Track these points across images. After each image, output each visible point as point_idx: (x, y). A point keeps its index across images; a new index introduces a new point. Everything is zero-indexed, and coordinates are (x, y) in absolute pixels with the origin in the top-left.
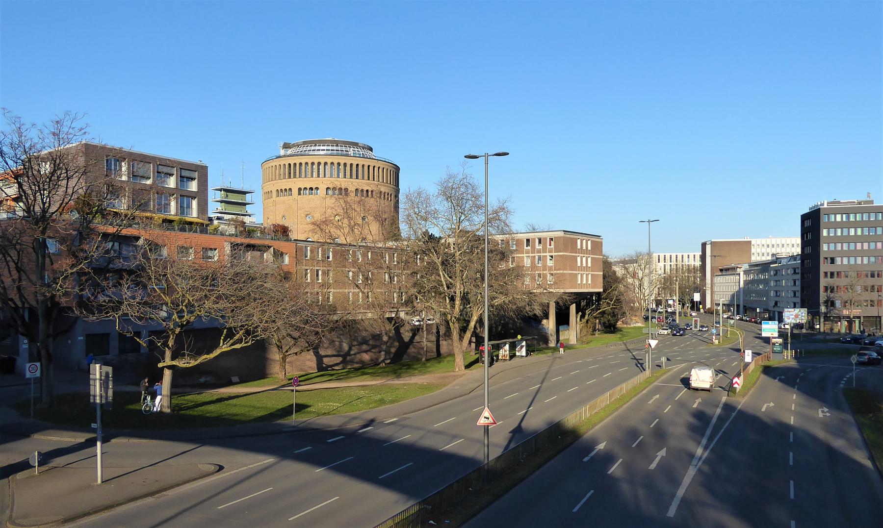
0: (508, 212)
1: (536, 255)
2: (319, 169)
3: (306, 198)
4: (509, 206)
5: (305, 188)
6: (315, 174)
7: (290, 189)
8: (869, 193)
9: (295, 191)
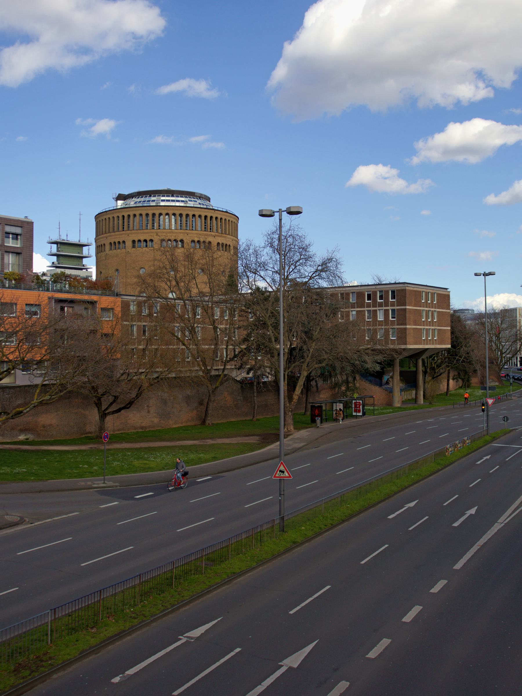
0: (337, 263)
1: (390, 308)
2: (153, 220)
3: (142, 250)
4: (337, 256)
5: (139, 241)
6: (150, 226)
7: (124, 242)
8: (476, 275)
9: (129, 244)
